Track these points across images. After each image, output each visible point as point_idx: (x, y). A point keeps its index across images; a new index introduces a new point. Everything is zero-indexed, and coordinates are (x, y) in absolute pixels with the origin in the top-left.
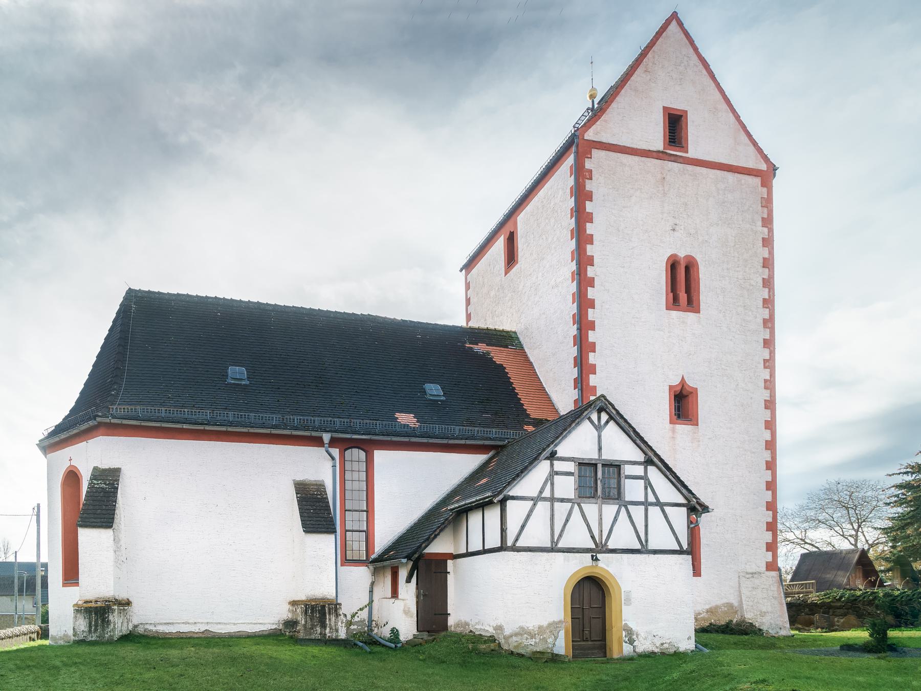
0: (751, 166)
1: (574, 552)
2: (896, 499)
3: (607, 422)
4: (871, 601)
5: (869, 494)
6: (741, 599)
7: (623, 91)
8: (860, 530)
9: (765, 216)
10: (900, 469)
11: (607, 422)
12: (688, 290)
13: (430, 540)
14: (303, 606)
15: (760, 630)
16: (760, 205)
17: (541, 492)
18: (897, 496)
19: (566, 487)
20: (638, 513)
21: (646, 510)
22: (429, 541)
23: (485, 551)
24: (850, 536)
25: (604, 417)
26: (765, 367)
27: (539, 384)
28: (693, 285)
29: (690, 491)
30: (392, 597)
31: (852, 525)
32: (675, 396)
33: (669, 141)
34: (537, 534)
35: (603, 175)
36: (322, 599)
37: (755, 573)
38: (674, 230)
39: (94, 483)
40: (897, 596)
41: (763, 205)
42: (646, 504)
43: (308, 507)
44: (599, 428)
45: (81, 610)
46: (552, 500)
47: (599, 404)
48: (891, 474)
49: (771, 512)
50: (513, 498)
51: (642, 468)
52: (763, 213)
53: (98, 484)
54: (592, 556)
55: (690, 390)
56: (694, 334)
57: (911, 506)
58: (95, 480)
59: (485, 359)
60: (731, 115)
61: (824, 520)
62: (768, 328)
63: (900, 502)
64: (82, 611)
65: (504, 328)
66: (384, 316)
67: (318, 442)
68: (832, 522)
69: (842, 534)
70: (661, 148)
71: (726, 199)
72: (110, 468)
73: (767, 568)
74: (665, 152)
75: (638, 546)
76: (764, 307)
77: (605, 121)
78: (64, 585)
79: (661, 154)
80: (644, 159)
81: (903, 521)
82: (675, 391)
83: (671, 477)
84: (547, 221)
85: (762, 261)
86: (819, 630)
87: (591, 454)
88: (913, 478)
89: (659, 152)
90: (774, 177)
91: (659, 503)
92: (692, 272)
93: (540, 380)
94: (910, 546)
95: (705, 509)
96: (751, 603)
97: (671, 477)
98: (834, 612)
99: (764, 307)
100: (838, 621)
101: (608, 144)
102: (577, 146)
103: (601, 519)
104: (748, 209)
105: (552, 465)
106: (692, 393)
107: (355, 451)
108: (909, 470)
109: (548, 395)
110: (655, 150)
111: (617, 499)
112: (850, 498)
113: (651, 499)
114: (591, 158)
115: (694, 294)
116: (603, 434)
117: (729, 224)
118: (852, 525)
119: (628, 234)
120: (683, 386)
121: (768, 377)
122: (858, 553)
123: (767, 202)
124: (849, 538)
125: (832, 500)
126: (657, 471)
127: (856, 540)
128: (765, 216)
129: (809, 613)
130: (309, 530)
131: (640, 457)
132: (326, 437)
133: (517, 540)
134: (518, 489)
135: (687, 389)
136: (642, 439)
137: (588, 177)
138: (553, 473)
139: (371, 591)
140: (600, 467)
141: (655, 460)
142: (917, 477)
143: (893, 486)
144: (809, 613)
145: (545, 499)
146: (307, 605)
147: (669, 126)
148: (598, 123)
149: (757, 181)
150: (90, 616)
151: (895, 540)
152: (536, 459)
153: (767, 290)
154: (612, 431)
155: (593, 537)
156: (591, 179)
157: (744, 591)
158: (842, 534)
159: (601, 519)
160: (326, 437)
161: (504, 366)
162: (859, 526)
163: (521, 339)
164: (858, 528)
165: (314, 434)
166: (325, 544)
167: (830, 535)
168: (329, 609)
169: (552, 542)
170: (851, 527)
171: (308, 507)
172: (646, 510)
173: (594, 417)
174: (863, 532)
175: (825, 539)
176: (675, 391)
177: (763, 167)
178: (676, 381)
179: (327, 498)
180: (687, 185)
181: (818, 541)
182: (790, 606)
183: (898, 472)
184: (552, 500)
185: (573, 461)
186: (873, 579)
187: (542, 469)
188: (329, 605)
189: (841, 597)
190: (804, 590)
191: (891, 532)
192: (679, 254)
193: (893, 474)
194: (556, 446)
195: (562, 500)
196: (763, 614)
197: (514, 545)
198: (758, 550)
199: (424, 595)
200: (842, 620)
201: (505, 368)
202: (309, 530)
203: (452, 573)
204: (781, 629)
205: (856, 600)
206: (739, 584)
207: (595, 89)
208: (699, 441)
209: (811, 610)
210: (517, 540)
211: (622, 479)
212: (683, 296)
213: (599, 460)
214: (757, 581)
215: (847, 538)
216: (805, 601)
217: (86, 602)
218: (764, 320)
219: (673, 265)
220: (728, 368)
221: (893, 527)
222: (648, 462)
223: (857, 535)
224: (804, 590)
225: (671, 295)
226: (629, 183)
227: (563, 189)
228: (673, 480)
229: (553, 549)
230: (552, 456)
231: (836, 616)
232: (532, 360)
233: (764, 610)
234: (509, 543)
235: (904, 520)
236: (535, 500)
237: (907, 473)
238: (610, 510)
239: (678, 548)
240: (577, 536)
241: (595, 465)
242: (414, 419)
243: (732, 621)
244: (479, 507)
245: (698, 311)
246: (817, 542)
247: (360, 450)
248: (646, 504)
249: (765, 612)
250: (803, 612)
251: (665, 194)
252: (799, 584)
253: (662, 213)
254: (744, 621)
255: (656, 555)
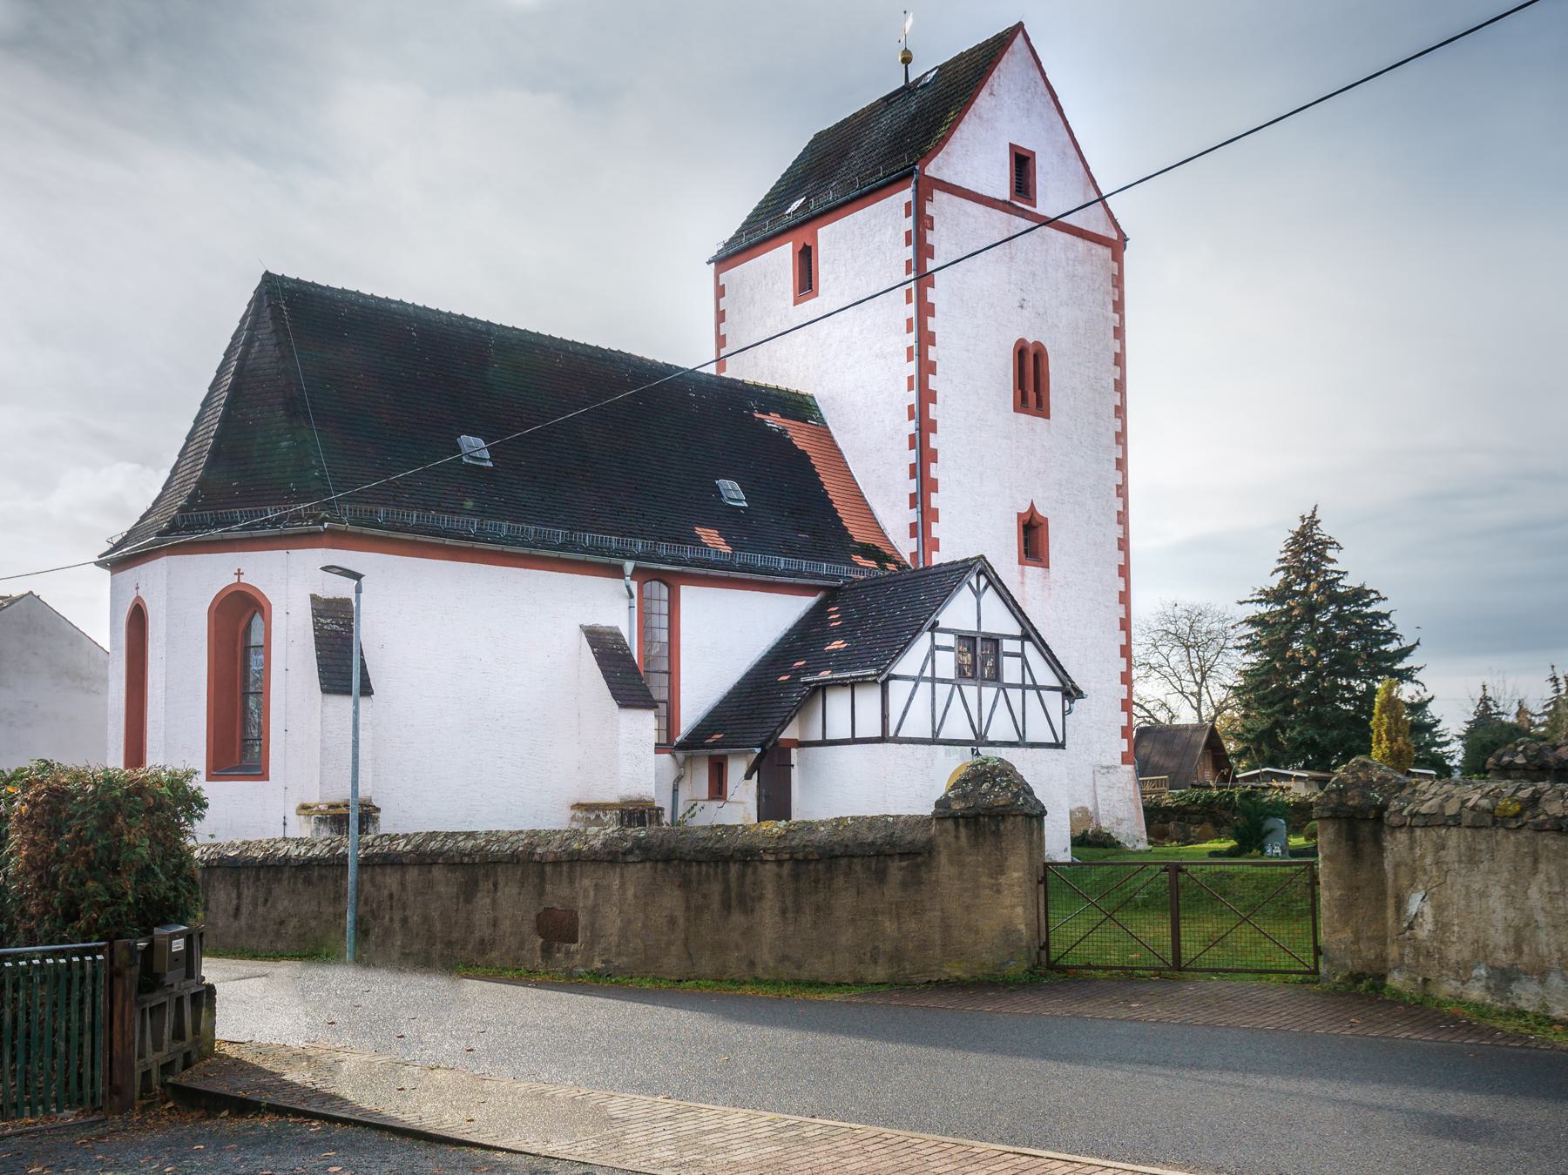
0: (1101, 234)
1: (955, 745)
2: (1248, 641)
3: (986, 587)
4: (1227, 803)
5: (1216, 626)
6: (1096, 801)
7: (966, 117)
8: (1204, 684)
9: (1117, 299)
10: (1253, 595)
11: (986, 587)
12: (1037, 388)
13: (786, 723)
14: (618, 812)
15: (1119, 843)
16: (1111, 284)
17: (922, 671)
18: (1249, 636)
19: (946, 664)
20: (1015, 695)
21: (1024, 694)
22: (784, 725)
23: (854, 741)
24: (1192, 694)
25: (983, 581)
26: (1118, 495)
27: (853, 486)
28: (1042, 381)
29: (1065, 673)
30: (711, 798)
31: (1194, 675)
32: (1024, 526)
33: (1017, 191)
34: (918, 724)
35: (945, 225)
36: (638, 801)
37: (1111, 767)
38: (1022, 307)
39: (322, 623)
40: (1216, 797)
41: (1115, 284)
42: (1023, 687)
43: (613, 669)
44: (978, 594)
45: (327, 818)
46: (933, 680)
47: (979, 567)
48: (1242, 601)
49: (1126, 686)
50: (896, 677)
51: (1019, 643)
52: (1114, 294)
53: (327, 624)
54: (973, 750)
55: (1040, 521)
56: (1043, 446)
57: (1267, 654)
58: (321, 617)
59: (781, 438)
60: (1080, 163)
61: (1157, 666)
62: (1121, 444)
63: (1251, 648)
64: (328, 820)
65: (799, 390)
66: (639, 355)
67: (617, 572)
68: (1168, 669)
69: (1180, 690)
70: (1007, 198)
71: (1076, 272)
72: (335, 598)
73: (1122, 761)
74: (1012, 204)
75: (1016, 738)
76: (1116, 417)
77: (948, 153)
78: (263, 775)
79: (1007, 206)
80: (989, 209)
81: (1257, 678)
82: (1024, 521)
83: (1047, 655)
84: (868, 259)
85: (1113, 357)
86: (1175, 843)
87: (969, 625)
88: (1268, 611)
89: (1005, 202)
90: (1125, 249)
91: (1037, 688)
92: (1040, 363)
93: (854, 480)
94: (1276, 640)
95: (1080, 694)
96: (1107, 808)
97: (1047, 655)
98: (1189, 819)
99: (1116, 417)
100: (1194, 831)
101: (951, 184)
102: (917, 183)
103: (980, 704)
104: (1099, 288)
105: (933, 638)
106: (1041, 524)
107: (656, 584)
108: (1263, 597)
109: (868, 505)
110: (1001, 199)
111: (995, 680)
112: (1190, 629)
113: (1028, 681)
114: (932, 201)
115: (1043, 394)
116: (982, 601)
117: (1079, 305)
118: (1194, 675)
119: (972, 307)
120: (1032, 514)
121: (1121, 509)
122: (1207, 732)
123: (1118, 281)
124: (1191, 697)
125: (1168, 633)
126: (1033, 647)
127: (1199, 701)
128: (1117, 299)
129: (1163, 820)
130: (625, 703)
131: (1016, 630)
132: (629, 566)
133: (898, 729)
134: (899, 668)
135: (1037, 518)
136: (1019, 609)
137: (929, 226)
138: (935, 648)
139: (675, 791)
140: (979, 640)
141: (1033, 634)
142: (1273, 610)
143: (1245, 621)
144: (1163, 820)
145: (926, 679)
146: (623, 810)
147: (1016, 170)
148: (940, 155)
149: (1107, 252)
150: (339, 828)
151: (1247, 705)
152: (919, 630)
153: (1119, 394)
154: (990, 597)
155: (973, 727)
156: (932, 229)
157: (1099, 791)
158: (1180, 690)
159: (980, 704)
160: (629, 566)
161: (809, 454)
162: (1203, 679)
163: (823, 410)
164: (1202, 682)
165: (615, 561)
166: (644, 725)
167: (1166, 692)
168: (650, 816)
169: (933, 731)
170: (1192, 679)
171: (613, 669)
172: (1024, 694)
173: (973, 581)
174: (1207, 688)
175: (1157, 696)
176: (1024, 521)
177: (1114, 235)
178: (1025, 509)
179: (631, 655)
180: (1035, 250)
181: (1149, 699)
182: (1145, 809)
183: (1250, 599)
184: (933, 680)
185: (953, 633)
186: (1226, 772)
187: (923, 643)
188: (649, 810)
189: (1197, 799)
190: (1156, 789)
191: (1243, 694)
192: (1028, 340)
193: (1245, 602)
194: (937, 615)
195: (943, 681)
196: (1119, 821)
197: (896, 735)
198: (1114, 737)
199: (767, 797)
200: (1198, 830)
201: (809, 457)
202: (625, 703)
203: (796, 766)
204: (1138, 841)
205: (1212, 802)
206: (1094, 781)
207: (909, 52)
208: (1050, 589)
209: (1165, 816)
210: (898, 729)
211: (1001, 656)
212: (1032, 395)
213: (979, 632)
214: (1113, 778)
215: (1187, 697)
216: (1157, 804)
217: (331, 807)
218: (1116, 433)
219: (1021, 351)
220: (1080, 494)
221: (1245, 686)
222: (1025, 637)
223: (1200, 694)
224: (1156, 789)
225: (1019, 392)
226: (973, 239)
227: (894, 228)
228: (1049, 659)
229: (935, 741)
230: (934, 628)
231: (1192, 824)
232: (840, 446)
233: (1121, 816)
234: (891, 734)
235: (1259, 675)
236: (917, 680)
237: (1260, 601)
238: (989, 692)
239: (1054, 741)
240: (957, 726)
241: (975, 639)
242: (726, 547)
243: (1087, 831)
244: (845, 685)
245: (1047, 416)
246: (1146, 702)
247: (662, 585)
248: (1023, 687)
249: (1121, 819)
250: (1155, 820)
251: (1012, 258)
252: (1150, 780)
253: (1009, 283)
254: (1100, 832)
255: (1034, 749)
